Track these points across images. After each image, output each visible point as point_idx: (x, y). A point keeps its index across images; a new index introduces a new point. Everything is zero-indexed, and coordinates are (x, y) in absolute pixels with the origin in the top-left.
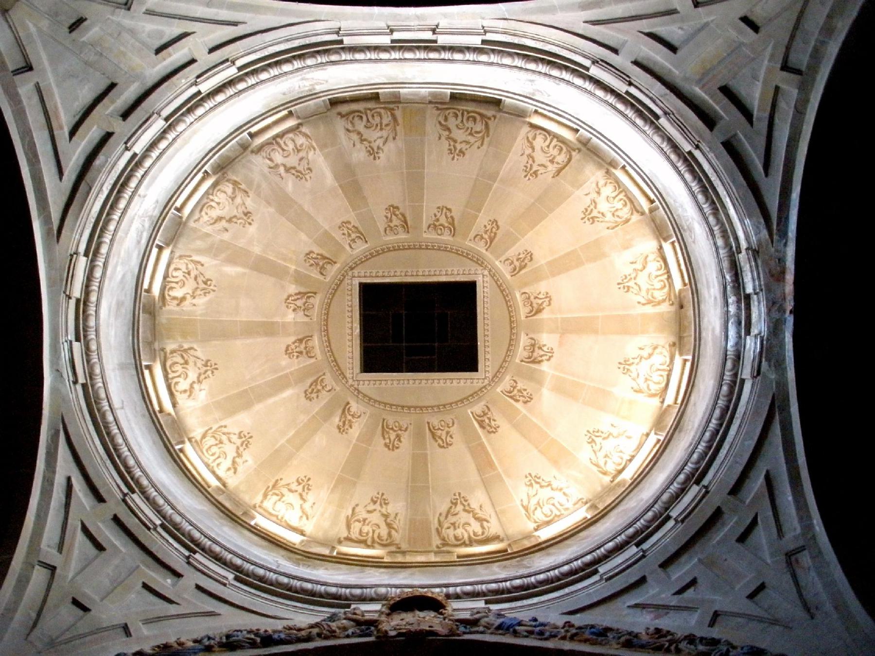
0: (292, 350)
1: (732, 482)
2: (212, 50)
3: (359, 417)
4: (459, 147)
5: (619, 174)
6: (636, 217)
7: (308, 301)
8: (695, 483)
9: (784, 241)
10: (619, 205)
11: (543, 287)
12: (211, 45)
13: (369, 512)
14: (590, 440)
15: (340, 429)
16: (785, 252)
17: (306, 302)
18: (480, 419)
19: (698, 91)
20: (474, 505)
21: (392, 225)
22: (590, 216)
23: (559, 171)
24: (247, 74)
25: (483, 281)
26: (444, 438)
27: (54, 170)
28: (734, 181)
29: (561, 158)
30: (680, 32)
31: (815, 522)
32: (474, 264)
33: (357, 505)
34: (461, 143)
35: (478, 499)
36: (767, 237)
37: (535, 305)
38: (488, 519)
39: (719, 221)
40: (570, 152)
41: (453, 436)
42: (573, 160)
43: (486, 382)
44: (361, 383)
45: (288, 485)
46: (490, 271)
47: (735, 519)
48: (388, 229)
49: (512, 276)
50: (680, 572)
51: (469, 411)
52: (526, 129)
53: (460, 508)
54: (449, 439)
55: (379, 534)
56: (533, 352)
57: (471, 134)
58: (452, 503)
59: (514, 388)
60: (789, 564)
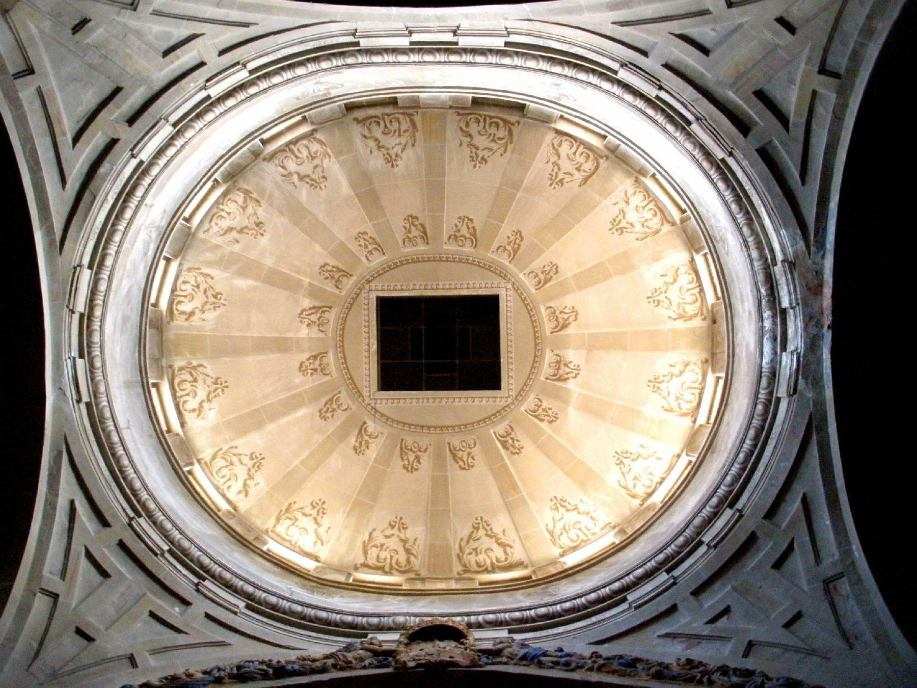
0: (306, 367)
2: (222, 53)
3: (376, 437)
4: (480, 154)
5: (649, 182)
6: (666, 228)
7: (323, 315)
9: (822, 253)
10: (649, 215)
12: (222, 47)
13: (387, 537)
16: (822, 264)
18: (503, 439)
19: (731, 96)
20: (497, 530)
21: (411, 236)
22: (618, 227)
23: (586, 180)
24: (259, 78)
26: (465, 459)
27: (57, 178)
29: (588, 166)
30: (713, 34)
31: (854, 547)
32: (497, 277)
33: (374, 530)
34: (483, 150)
35: (501, 523)
36: (804, 248)
37: (561, 320)
38: (512, 544)
39: (753, 232)
40: (597, 160)
41: (475, 458)
42: (600, 168)
44: (379, 401)
45: (302, 508)
47: (770, 544)
48: (407, 240)
49: (536, 289)
50: (713, 600)
51: (492, 431)
52: (551, 135)
53: (482, 532)
54: (470, 460)
56: (558, 369)
57: (493, 141)
58: (474, 527)
59: (539, 406)
60: (827, 591)
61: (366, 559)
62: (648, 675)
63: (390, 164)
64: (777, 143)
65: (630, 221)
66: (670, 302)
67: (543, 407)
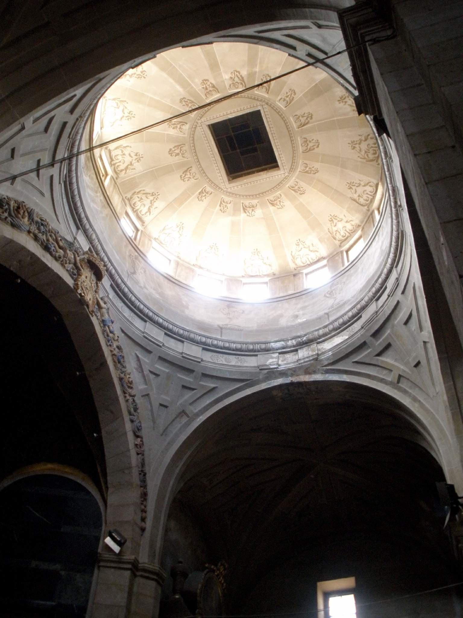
0: (206, 83)
1: (207, 373)
3: (181, 132)
4: (357, 146)
5: (359, 233)
6: (337, 243)
7: (239, 84)
8: (203, 347)
9: (324, 373)
10: (342, 233)
11: (287, 203)
13: (130, 155)
14: (212, 246)
15: (170, 151)
16: (318, 373)
17: (238, 83)
18: (203, 191)
19: (388, 332)
20: (156, 204)
21: (301, 118)
22: (333, 219)
23: (354, 200)
25: (281, 174)
26: (186, 176)
28: (348, 346)
29: (362, 201)
30: (413, 329)
31: (201, 417)
32: (290, 167)
33: (131, 147)
34: (360, 147)
35: (160, 204)
36: (325, 364)
37: (276, 202)
38: (152, 213)
39: (331, 331)
40: (366, 205)
41: (189, 181)
42: (362, 207)
43: (225, 190)
44: (201, 127)
45: (126, 108)
46: (288, 176)
47: (191, 380)
48: (297, 117)
49: (289, 187)
50: (161, 367)
51: (206, 185)
52: (375, 182)
53: (152, 198)
54: (187, 179)
55: (120, 165)
56: (249, 207)
57: (366, 152)
58: (153, 193)
59: (227, 203)
60: (180, 413)
61: (113, 150)
62: (119, 375)
63: (339, 99)
64: (369, 350)
65: (337, 224)
66: (300, 250)
67: (227, 205)
